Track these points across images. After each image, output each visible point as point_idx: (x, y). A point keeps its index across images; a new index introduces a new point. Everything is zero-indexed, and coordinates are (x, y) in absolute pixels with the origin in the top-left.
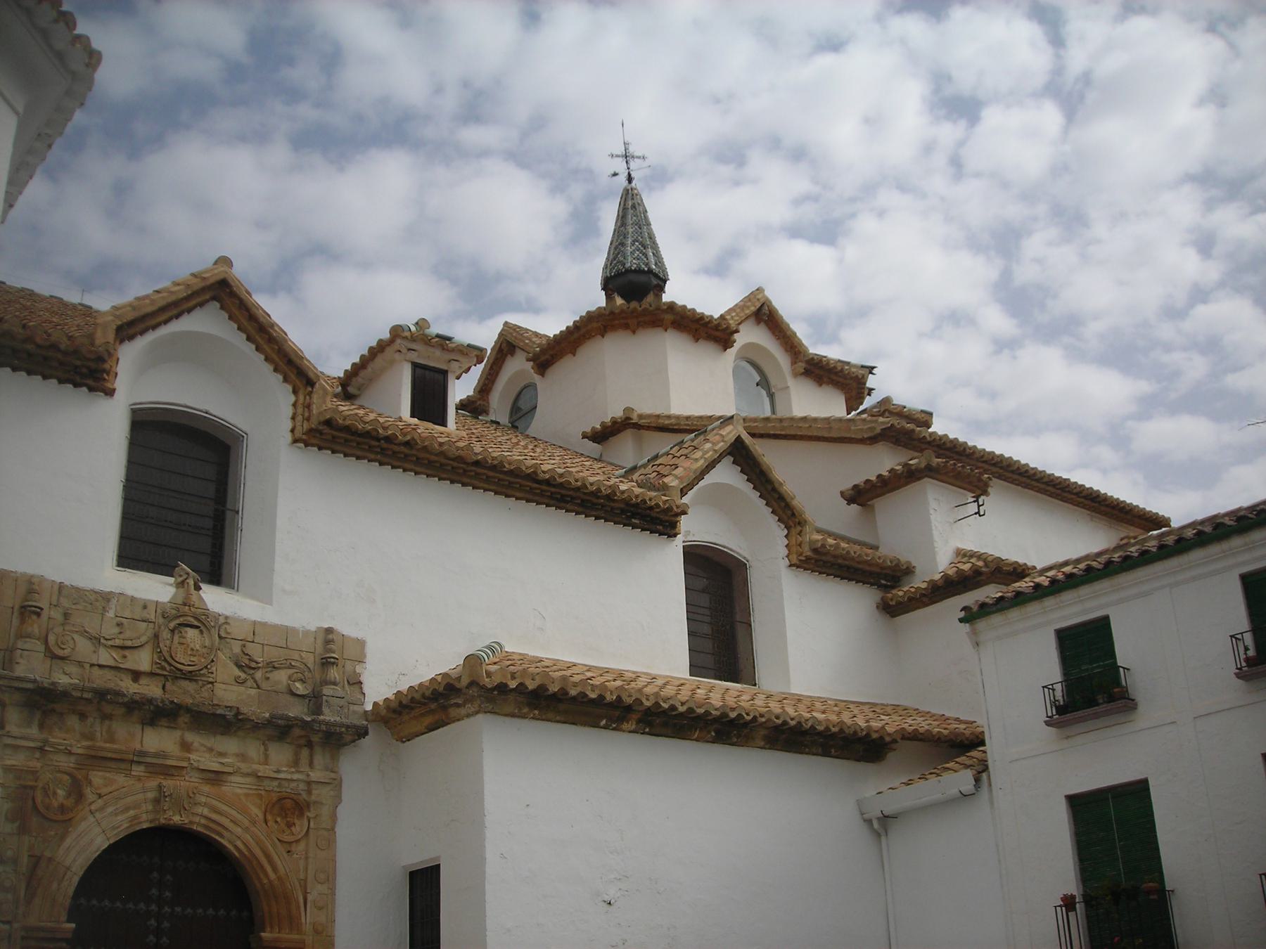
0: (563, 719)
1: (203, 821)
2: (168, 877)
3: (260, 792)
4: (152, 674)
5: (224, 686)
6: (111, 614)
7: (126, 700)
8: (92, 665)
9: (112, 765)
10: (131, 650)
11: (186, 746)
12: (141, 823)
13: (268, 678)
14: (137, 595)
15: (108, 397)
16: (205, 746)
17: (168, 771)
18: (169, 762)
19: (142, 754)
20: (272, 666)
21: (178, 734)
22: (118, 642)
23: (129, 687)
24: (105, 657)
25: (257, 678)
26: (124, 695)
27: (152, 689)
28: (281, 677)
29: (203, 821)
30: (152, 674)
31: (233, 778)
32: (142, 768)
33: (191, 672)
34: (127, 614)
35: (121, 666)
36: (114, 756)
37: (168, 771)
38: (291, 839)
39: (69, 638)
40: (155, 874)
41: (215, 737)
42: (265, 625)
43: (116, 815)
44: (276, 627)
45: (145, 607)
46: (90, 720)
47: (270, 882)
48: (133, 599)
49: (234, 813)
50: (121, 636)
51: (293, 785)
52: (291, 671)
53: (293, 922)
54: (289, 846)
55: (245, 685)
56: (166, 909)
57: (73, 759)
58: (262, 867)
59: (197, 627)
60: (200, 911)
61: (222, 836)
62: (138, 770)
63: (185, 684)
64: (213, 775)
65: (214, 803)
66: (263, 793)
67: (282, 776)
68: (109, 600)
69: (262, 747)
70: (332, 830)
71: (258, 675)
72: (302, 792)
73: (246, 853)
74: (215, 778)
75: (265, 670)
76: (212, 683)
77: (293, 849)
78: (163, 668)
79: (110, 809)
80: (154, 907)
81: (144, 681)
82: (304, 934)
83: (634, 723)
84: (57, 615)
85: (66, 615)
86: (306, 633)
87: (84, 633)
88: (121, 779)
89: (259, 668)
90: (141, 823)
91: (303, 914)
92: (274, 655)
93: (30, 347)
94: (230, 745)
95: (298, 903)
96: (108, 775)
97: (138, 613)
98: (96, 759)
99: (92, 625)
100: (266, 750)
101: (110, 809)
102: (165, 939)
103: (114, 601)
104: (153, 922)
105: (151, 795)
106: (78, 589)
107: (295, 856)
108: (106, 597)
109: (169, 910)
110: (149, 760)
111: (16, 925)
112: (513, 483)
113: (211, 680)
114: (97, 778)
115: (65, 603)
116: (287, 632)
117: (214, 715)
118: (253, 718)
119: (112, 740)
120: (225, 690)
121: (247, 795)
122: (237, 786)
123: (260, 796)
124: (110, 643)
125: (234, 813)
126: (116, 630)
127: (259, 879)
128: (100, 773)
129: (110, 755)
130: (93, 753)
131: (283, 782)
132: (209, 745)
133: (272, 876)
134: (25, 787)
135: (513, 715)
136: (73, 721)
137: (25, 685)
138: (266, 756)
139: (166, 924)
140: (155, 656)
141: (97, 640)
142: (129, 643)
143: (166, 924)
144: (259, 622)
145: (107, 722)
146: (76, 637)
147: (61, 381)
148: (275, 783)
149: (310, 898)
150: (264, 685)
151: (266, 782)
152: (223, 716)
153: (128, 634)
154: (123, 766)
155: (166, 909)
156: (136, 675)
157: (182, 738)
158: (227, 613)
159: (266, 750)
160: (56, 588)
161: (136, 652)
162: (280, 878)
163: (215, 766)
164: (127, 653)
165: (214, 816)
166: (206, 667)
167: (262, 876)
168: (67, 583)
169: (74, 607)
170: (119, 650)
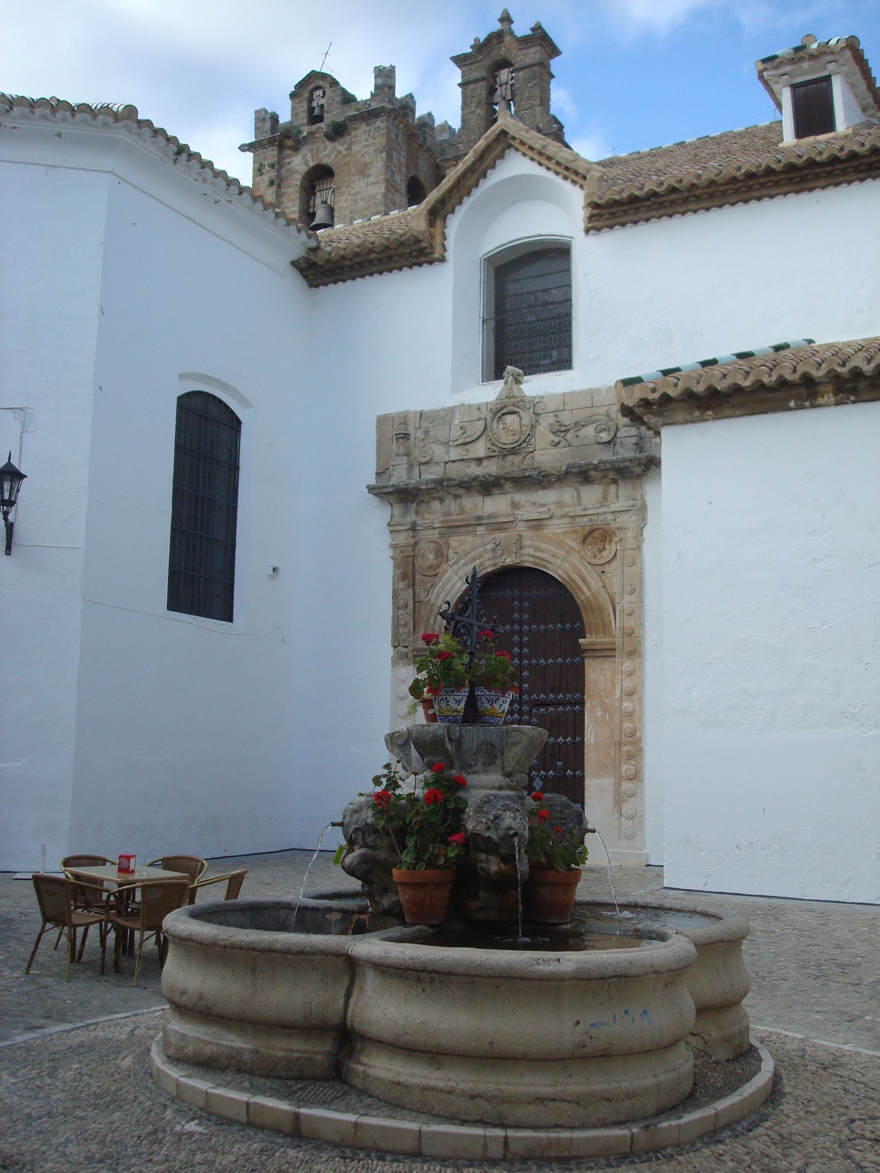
0: (744, 412)
1: (531, 559)
2: (526, 604)
3: (575, 528)
4: (490, 457)
5: (541, 452)
6: (456, 422)
7: (456, 482)
8: (446, 463)
9: (463, 530)
10: (470, 445)
11: (515, 505)
12: (486, 568)
13: (577, 436)
14: (473, 402)
15: (444, 263)
16: (530, 502)
17: (501, 527)
18: (500, 520)
19: (479, 518)
20: (579, 425)
21: (509, 496)
22: (460, 441)
23: (475, 470)
24: (455, 454)
25: (568, 439)
26: (454, 480)
27: (491, 468)
28: (589, 432)
29: (531, 559)
30: (490, 457)
31: (555, 522)
32: (483, 528)
33: (513, 448)
34: (467, 419)
35: (465, 458)
36: (462, 524)
37: (501, 527)
38: (602, 561)
39: (428, 448)
40: (516, 603)
41: (483, 496)
42: (572, 394)
43: (467, 565)
44: (582, 393)
45: (479, 409)
46: (447, 501)
47: (587, 598)
48: (470, 406)
49: (553, 549)
50: (464, 436)
51: (601, 517)
52: (595, 425)
53: (606, 628)
54: (601, 570)
55: (559, 446)
56: (525, 627)
57: (437, 531)
58: (577, 585)
59: (516, 412)
60: (551, 626)
61: (548, 569)
62: (481, 530)
63: (510, 458)
64: (535, 523)
65: (537, 543)
66: (578, 528)
67: (590, 512)
68: (454, 412)
69: (576, 492)
70: (639, 548)
71: (569, 435)
72: (611, 522)
73: (567, 578)
74: (537, 524)
75: (573, 430)
76: (532, 452)
77: (606, 570)
78: (494, 451)
79: (462, 562)
80: (516, 627)
81: (485, 463)
82: (615, 637)
83: (831, 395)
84: (420, 434)
85: (427, 433)
86: (608, 389)
87: (437, 441)
88: (469, 539)
89: (569, 430)
90: (486, 568)
91: (613, 621)
92: (580, 416)
93: (373, 256)
94: (548, 496)
95: (608, 613)
96: (461, 538)
97: (475, 415)
98: (450, 528)
99: (441, 433)
100: (579, 494)
101: (462, 562)
102: (525, 649)
103: (457, 412)
104: (516, 638)
105: (489, 547)
106: (432, 412)
107: (608, 575)
108: (451, 411)
109: (528, 628)
110: (485, 521)
111: (410, 648)
112: (846, 168)
113: (531, 450)
114: (454, 541)
115: (425, 424)
116: (591, 394)
117: (524, 477)
118: (554, 472)
119: (462, 512)
120: (543, 455)
121: (564, 533)
122: (556, 527)
123: (576, 532)
124: (456, 443)
125: (553, 549)
126: (460, 432)
127: (579, 597)
128: (456, 538)
129: (458, 524)
130: (446, 525)
131: (593, 517)
132: (533, 501)
133: (587, 593)
134: (406, 557)
135: (686, 422)
136: (436, 505)
137: (387, 490)
138: (579, 499)
139: (526, 638)
140: (488, 443)
141: (446, 444)
142: (468, 440)
143: (526, 638)
144: (568, 393)
145: (458, 500)
146: (433, 446)
147: (410, 267)
148: (586, 519)
149: (618, 607)
150: (574, 442)
151: (579, 519)
152: (531, 476)
153: (468, 433)
154: (469, 529)
155: (525, 627)
156: (479, 460)
157: (512, 500)
158: (541, 394)
159: (579, 494)
160: (419, 415)
161: (474, 444)
162: (593, 594)
163: (535, 516)
164: (468, 447)
165: (538, 554)
166: (524, 441)
167: (580, 594)
168: (426, 410)
169: (431, 425)
170: (463, 447)
